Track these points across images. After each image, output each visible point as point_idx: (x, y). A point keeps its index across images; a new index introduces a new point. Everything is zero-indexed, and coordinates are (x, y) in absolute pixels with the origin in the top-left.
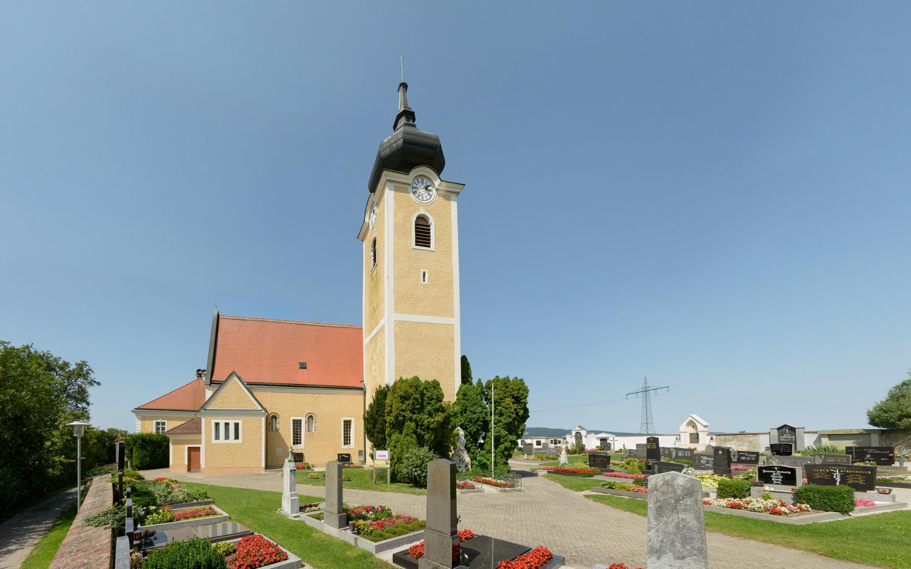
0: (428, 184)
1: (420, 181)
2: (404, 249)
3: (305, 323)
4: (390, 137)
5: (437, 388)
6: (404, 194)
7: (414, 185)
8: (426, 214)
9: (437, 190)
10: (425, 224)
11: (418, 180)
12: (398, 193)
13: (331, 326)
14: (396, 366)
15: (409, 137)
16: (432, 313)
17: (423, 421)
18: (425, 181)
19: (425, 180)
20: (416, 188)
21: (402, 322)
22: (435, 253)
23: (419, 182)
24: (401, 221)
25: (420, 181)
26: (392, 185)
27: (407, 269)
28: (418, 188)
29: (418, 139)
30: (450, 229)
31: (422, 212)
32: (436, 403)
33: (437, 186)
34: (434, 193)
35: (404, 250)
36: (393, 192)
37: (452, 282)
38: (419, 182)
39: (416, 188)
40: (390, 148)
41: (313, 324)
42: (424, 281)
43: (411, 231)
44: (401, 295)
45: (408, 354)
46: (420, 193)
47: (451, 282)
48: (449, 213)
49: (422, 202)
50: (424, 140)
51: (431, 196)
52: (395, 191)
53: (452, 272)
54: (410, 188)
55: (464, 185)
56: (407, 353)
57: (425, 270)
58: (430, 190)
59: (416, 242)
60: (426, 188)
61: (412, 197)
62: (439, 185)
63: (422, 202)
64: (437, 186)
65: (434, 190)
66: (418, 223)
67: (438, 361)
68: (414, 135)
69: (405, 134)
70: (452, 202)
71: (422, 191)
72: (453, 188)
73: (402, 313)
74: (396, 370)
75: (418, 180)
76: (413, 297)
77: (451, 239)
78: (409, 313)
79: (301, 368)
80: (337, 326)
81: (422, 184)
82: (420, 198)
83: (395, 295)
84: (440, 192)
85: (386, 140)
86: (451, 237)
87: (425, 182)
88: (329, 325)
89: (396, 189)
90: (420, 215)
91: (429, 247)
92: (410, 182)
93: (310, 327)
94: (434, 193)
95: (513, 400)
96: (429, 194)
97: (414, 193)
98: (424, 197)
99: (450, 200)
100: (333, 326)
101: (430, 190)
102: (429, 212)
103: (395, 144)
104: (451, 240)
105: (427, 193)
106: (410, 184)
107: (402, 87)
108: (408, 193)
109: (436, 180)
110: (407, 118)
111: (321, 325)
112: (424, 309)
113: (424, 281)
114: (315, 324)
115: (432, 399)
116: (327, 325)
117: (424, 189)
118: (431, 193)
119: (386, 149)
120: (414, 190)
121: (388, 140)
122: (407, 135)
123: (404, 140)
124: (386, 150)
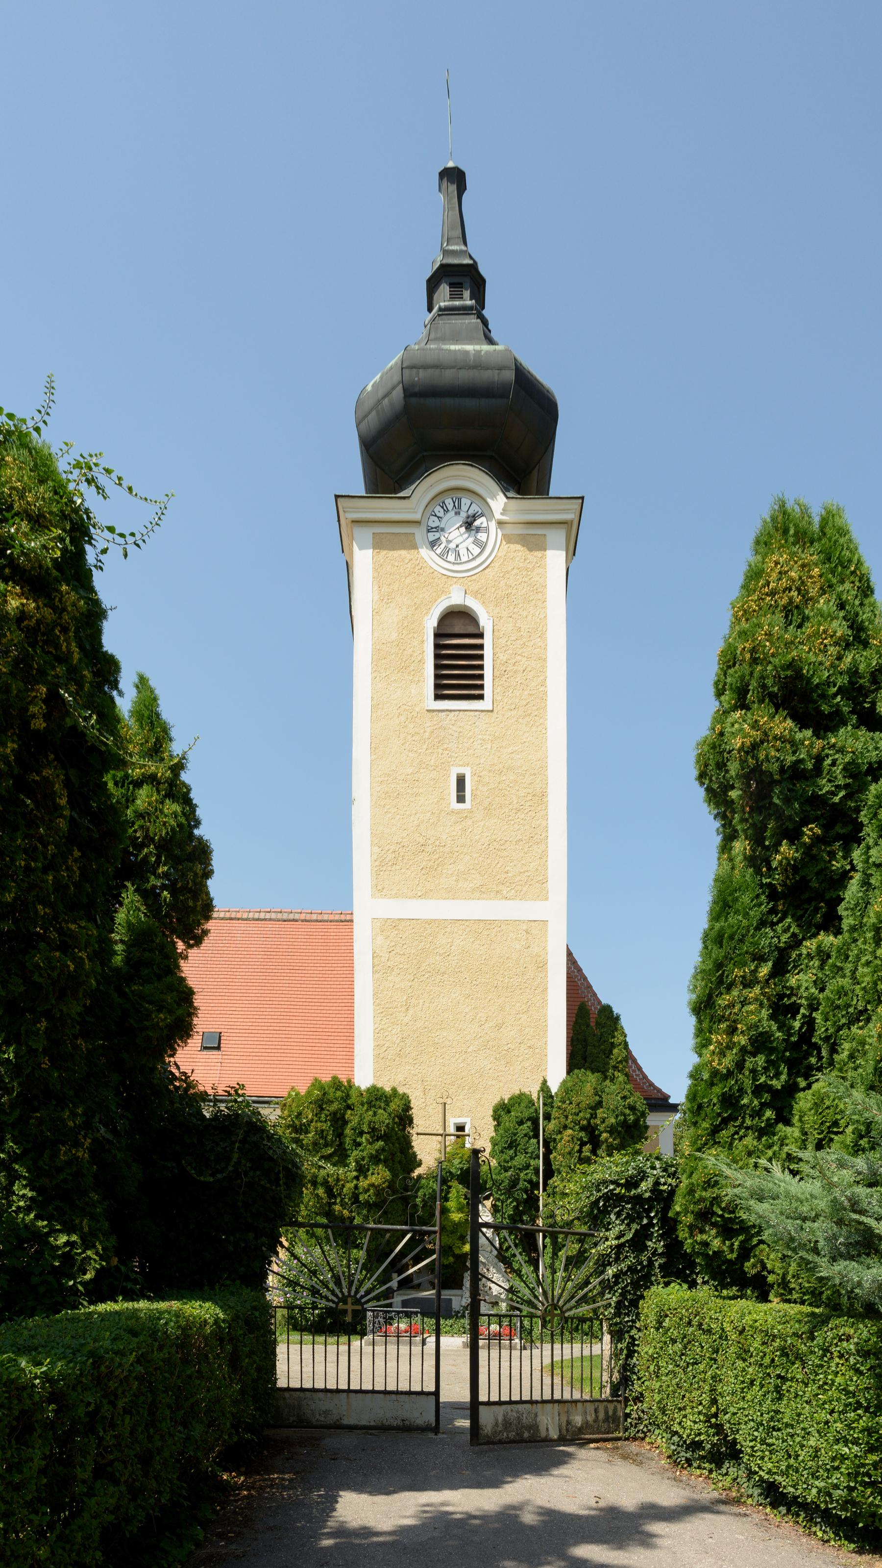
0: (475, 509)
1: (450, 507)
2: (400, 715)
3: (239, 916)
4: (378, 377)
5: (374, 1106)
6: (403, 552)
7: (434, 522)
8: (467, 603)
9: (500, 523)
10: (471, 630)
11: (443, 506)
12: (384, 552)
13: (314, 917)
14: (377, 1046)
15: (422, 377)
16: (481, 892)
17: (343, 1186)
18: (465, 502)
19: (463, 501)
20: (438, 529)
21: (394, 924)
22: (494, 715)
23: (446, 511)
24: (394, 635)
25: (450, 507)
26: (366, 534)
27: (409, 771)
28: (443, 530)
29: (448, 377)
30: (543, 636)
31: (456, 598)
32: (370, 1143)
33: (498, 516)
34: (493, 535)
35: (402, 718)
36: (370, 552)
37: (544, 795)
38: (446, 511)
39: (438, 529)
40: (378, 412)
41: (262, 916)
42: (461, 799)
43: (422, 661)
44: (392, 848)
45: (411, 1012)
46: (449, 542)
47: (541, 797)
48: (539, 590)
49: (456, 568)
50: (465, 377)
51: (483, 546)
52: (374, 548)
53: (544, 768)
54: (419, 534)
55: (582, 498)
56: (407, 1009)
57: (461, 770)
58: (478, 529)
59: (437, 686)
60: (469, 525)
61: (426, 558)
62: (504, 511)
63: (456, 568)
64: (498, 516)
65: (493, 525)
66: (441, 632)
67: (499, 1027)
68: (425, 367)
69: (406, 372)
70: (549, 553)
71: (455, 534)
72: (546, 512)
73: (396, 896)
74: (377, 1057)
75: (443, 506)
76: (429, 849)
77: (544, 667)
78: (415, 897)
79: (206, 1048)
80: (332, 917)
81: (457, 513)
82: (451, 557)
83: (376, 850)
84: (510, 530)
85: (369, 388)
86: (545, 660)
87: (464, 508)
88: (308, 917)
89: (379, 544)
90: (452, 606)
91: (481, 697)
92: (417, 517)
93: (252, 926)
94: (493, 535)
95: (582, 1134)
96: (477, 542)
97: (433, 544)
98: (463, 551)
99: (545, 550)
100: (320, 917)
101: (478, 529)
102: (476, 594)
103: (386, 400)
104: (543, 669)
105: (471, 539)
106: (417, 523)
107: (445, 180)
108: (414, 547)
109: (494, 497)
110: (451, 285)
111: (285, 916)
112: (457, 881)
113: (461, 799)
114: (268, 916)
115: (361, 1133)
116: (303, 917)
117: (463, 529)
118: (482, 536)
119: (369, 413)
120: (432, 536)
121: (373, 386)
122: (414, 371)
123: (405, 390)
124: (370, 417)
